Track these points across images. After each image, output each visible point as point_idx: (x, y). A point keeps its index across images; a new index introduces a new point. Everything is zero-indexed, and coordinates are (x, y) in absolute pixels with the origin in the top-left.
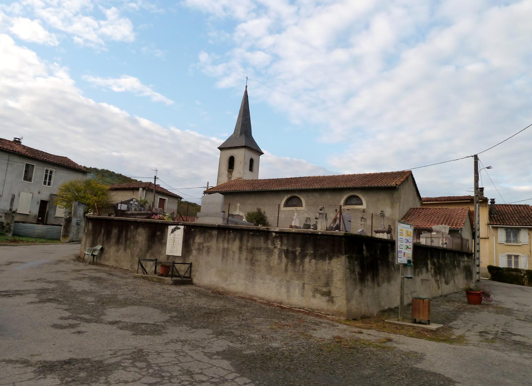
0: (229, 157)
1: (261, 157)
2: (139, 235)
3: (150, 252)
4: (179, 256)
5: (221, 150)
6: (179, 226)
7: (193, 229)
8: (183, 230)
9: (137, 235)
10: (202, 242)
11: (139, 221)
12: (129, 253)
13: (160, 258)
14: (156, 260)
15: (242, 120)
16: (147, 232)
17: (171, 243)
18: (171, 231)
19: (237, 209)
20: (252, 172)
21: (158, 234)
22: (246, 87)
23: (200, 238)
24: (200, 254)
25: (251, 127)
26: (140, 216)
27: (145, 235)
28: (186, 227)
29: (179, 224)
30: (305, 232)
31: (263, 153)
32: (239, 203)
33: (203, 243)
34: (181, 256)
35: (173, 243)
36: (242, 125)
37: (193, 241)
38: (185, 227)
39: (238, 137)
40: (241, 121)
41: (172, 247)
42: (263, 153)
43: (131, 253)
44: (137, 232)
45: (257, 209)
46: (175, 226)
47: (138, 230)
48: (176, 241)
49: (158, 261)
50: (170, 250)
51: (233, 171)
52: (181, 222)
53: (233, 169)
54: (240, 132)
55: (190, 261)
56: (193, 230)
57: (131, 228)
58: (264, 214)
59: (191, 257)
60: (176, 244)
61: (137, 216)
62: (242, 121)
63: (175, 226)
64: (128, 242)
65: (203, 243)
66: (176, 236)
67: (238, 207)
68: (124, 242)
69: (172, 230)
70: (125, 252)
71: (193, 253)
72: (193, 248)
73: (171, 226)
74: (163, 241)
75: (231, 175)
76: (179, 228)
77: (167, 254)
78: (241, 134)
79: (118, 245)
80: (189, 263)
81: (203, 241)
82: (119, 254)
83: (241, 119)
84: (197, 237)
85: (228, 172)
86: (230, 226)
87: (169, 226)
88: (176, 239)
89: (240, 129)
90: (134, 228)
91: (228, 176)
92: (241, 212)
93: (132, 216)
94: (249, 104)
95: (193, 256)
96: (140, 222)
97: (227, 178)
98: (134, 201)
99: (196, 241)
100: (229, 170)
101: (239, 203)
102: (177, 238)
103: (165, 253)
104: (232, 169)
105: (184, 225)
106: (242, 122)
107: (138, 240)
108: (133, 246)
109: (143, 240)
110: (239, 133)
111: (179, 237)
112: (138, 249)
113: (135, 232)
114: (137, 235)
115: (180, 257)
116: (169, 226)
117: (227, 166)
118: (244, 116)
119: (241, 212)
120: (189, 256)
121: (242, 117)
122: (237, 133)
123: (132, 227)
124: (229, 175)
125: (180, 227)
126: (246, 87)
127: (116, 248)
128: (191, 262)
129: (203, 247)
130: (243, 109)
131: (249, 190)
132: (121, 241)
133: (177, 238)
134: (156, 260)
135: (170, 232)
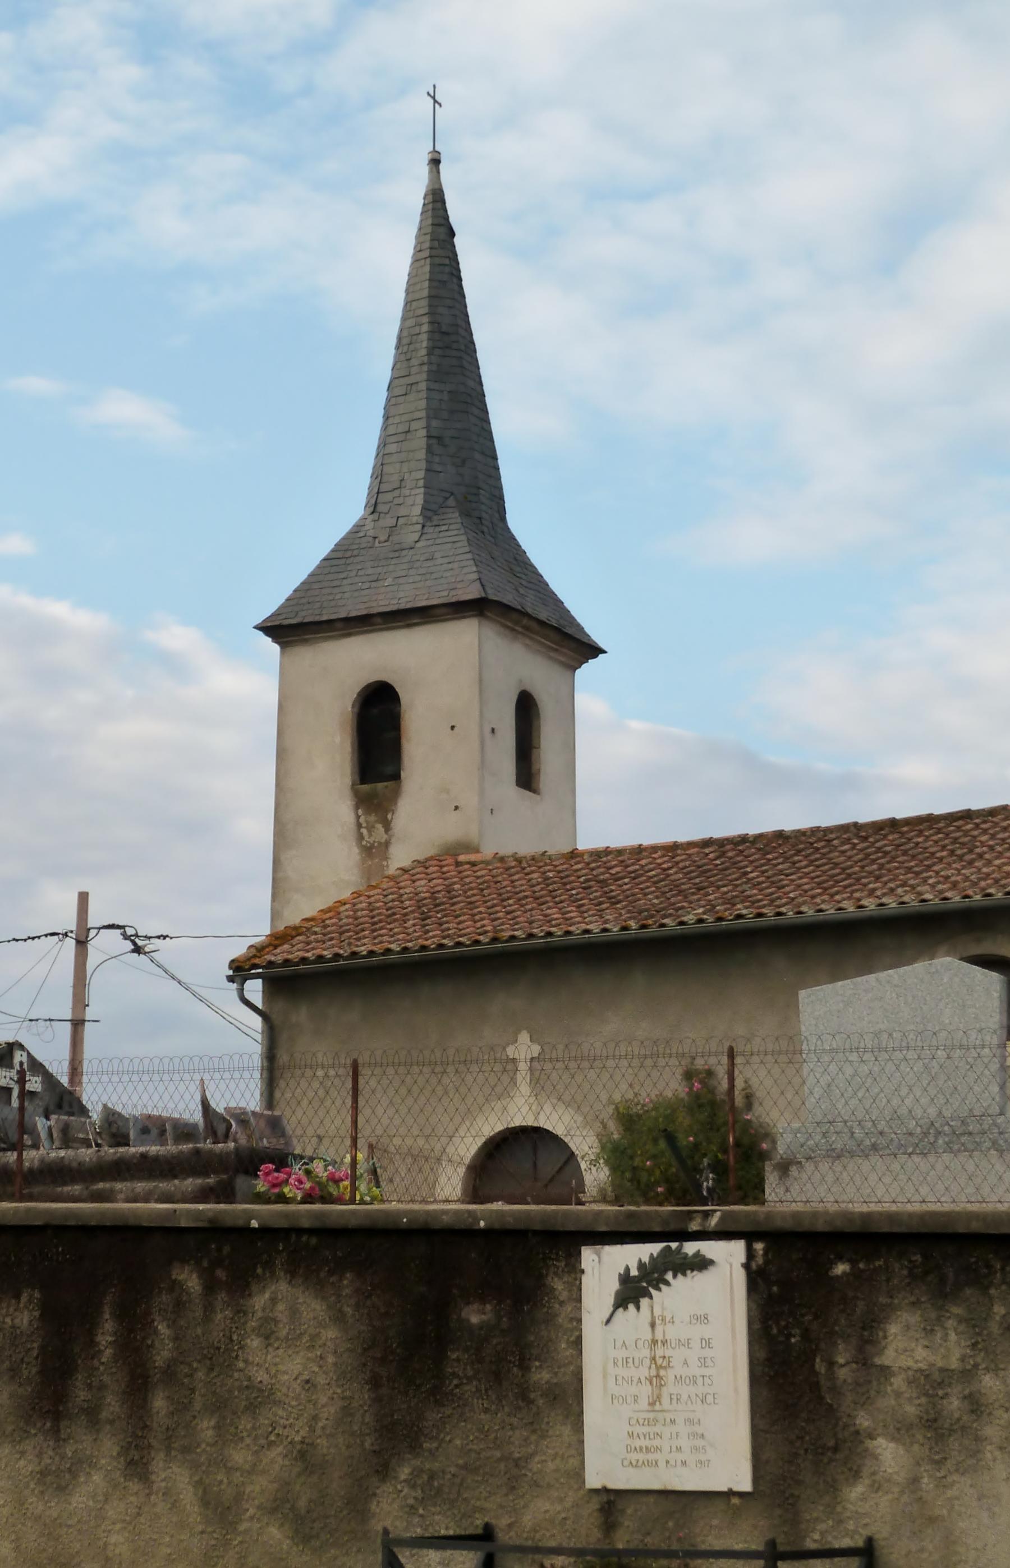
0: (358, 690)
1: (588, 672)
2: (268, 1337)
3: (404, 1472)
4: (731, 1493)
5: (282, 648)
6: (690, 1248)
7: (840, 1258)
8: (740, 1277)
9: (254, 1343)
10: (954, 1364)
11: (254, 1224)
12: (188, 1496)
13: (527, 1520)
14: (487, 1535)
15: (428, 409)
16: (348, 1310)
17: (633, 1390)
18: (615, 1285)
19: (513, 1080)
20: (539, 794)
21: (475, 1320)
22: (435, 162)
23: (929, 1332)
24: (949, 1464)
25: (495, 458)
26: (141, 1186)
27: (331, 1333)
28: (766, 1252)
29: (694, 1226)
30: (510, 1223)
31: (594, 651)
32: (524, 1037)
33: (968, 1374)
34: (745, 1485)
35: (645, 1391)
36: (429, 450)
37: (863, 1361)
38: (759, 1246)
39: (409, 535)
40: (423, 414)
41: (648, 1422)
42: (594, 651)
43: (207, 1500)
44: (241, 1311)
45: (689, 1075)
46: (655, 1248)
47: (259, 1301)
48: (678, 1369)
49: (504, 1537)
50: (629, 1449)
51: (396, 794)
52: (707, 1215)
53: (396, 777)
54: (420, 500)
55: (851, 1525)
56: (841, 1268)
57: (175, 1286)
58: (749, 1106)
59: (855, 1492)
60: (685, 1391)
61: (119, 1186)
62: (432, 414)
63: (648, 1251)
64: (159, 1403)
65: (968, 1374)
66: (672, 1333)
67: (523, 1066)
68: (112, 1405)
69: (625, 1279)
70: (134, 1486)
71: (876, 1457)
72: (863, 1421)
73: (608, 1249)
74: (541, 1376)
75: (387, 826)
76: (702, 1264)
77: (593, 1480)
78: (430, 513)
79: (56, 1431)
80: (846, 1543)
81: (963, 1359)
82: (79, 1500)
83: (418, 403)
84: (893, 1329)
85: (357, 807)
86: (435, 1211)
87: (588, 1255)
88: (677, 1355)
89: (421, 474)
90: (210, 1287)
91: (360, 837)
92: (548, 1108)
93: (67, 1189)
94: (465, 284)
95: (876, 1487)
96: (267, 1232)
97: (356, 850)
98: (17, 1067)
99: (889, 1357)
100: (366, 788)
101: (524, 1037)
102: (687, 1344)
103: (579, 1473)
104: (389, 784)
105: (749, 1237)
106: (428, 427)
107: (261, 1376)
108: (217, 1427)
109: (321, 1380)
110: (417, 510)
111: (707, 1331)
112: (276, 1458)
113: (222, 1316)
114: (254, 1343)
115: (735, 1501)
116: (588, 1255)
117: (352, 760)
118: (437, 375)
119: (548, 1108)
120: (833, 1488)
121: (428, 389)
122: (403, 511)
123: (191, 1281)
124: (370, 829)
125: (709, 1255)
126: (435, 162)
127: (40, 1455)
128: (865, 1533)
129: (976, 1405)
130: (425, 328)
131: (709, 918)
132: (81, 1395)
133: (687, 1344)
134: (487, 1535)
135: (611, 1300)
